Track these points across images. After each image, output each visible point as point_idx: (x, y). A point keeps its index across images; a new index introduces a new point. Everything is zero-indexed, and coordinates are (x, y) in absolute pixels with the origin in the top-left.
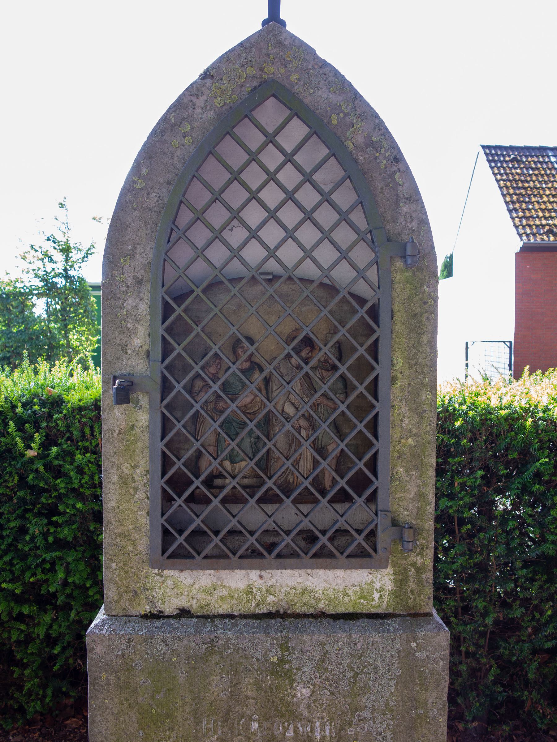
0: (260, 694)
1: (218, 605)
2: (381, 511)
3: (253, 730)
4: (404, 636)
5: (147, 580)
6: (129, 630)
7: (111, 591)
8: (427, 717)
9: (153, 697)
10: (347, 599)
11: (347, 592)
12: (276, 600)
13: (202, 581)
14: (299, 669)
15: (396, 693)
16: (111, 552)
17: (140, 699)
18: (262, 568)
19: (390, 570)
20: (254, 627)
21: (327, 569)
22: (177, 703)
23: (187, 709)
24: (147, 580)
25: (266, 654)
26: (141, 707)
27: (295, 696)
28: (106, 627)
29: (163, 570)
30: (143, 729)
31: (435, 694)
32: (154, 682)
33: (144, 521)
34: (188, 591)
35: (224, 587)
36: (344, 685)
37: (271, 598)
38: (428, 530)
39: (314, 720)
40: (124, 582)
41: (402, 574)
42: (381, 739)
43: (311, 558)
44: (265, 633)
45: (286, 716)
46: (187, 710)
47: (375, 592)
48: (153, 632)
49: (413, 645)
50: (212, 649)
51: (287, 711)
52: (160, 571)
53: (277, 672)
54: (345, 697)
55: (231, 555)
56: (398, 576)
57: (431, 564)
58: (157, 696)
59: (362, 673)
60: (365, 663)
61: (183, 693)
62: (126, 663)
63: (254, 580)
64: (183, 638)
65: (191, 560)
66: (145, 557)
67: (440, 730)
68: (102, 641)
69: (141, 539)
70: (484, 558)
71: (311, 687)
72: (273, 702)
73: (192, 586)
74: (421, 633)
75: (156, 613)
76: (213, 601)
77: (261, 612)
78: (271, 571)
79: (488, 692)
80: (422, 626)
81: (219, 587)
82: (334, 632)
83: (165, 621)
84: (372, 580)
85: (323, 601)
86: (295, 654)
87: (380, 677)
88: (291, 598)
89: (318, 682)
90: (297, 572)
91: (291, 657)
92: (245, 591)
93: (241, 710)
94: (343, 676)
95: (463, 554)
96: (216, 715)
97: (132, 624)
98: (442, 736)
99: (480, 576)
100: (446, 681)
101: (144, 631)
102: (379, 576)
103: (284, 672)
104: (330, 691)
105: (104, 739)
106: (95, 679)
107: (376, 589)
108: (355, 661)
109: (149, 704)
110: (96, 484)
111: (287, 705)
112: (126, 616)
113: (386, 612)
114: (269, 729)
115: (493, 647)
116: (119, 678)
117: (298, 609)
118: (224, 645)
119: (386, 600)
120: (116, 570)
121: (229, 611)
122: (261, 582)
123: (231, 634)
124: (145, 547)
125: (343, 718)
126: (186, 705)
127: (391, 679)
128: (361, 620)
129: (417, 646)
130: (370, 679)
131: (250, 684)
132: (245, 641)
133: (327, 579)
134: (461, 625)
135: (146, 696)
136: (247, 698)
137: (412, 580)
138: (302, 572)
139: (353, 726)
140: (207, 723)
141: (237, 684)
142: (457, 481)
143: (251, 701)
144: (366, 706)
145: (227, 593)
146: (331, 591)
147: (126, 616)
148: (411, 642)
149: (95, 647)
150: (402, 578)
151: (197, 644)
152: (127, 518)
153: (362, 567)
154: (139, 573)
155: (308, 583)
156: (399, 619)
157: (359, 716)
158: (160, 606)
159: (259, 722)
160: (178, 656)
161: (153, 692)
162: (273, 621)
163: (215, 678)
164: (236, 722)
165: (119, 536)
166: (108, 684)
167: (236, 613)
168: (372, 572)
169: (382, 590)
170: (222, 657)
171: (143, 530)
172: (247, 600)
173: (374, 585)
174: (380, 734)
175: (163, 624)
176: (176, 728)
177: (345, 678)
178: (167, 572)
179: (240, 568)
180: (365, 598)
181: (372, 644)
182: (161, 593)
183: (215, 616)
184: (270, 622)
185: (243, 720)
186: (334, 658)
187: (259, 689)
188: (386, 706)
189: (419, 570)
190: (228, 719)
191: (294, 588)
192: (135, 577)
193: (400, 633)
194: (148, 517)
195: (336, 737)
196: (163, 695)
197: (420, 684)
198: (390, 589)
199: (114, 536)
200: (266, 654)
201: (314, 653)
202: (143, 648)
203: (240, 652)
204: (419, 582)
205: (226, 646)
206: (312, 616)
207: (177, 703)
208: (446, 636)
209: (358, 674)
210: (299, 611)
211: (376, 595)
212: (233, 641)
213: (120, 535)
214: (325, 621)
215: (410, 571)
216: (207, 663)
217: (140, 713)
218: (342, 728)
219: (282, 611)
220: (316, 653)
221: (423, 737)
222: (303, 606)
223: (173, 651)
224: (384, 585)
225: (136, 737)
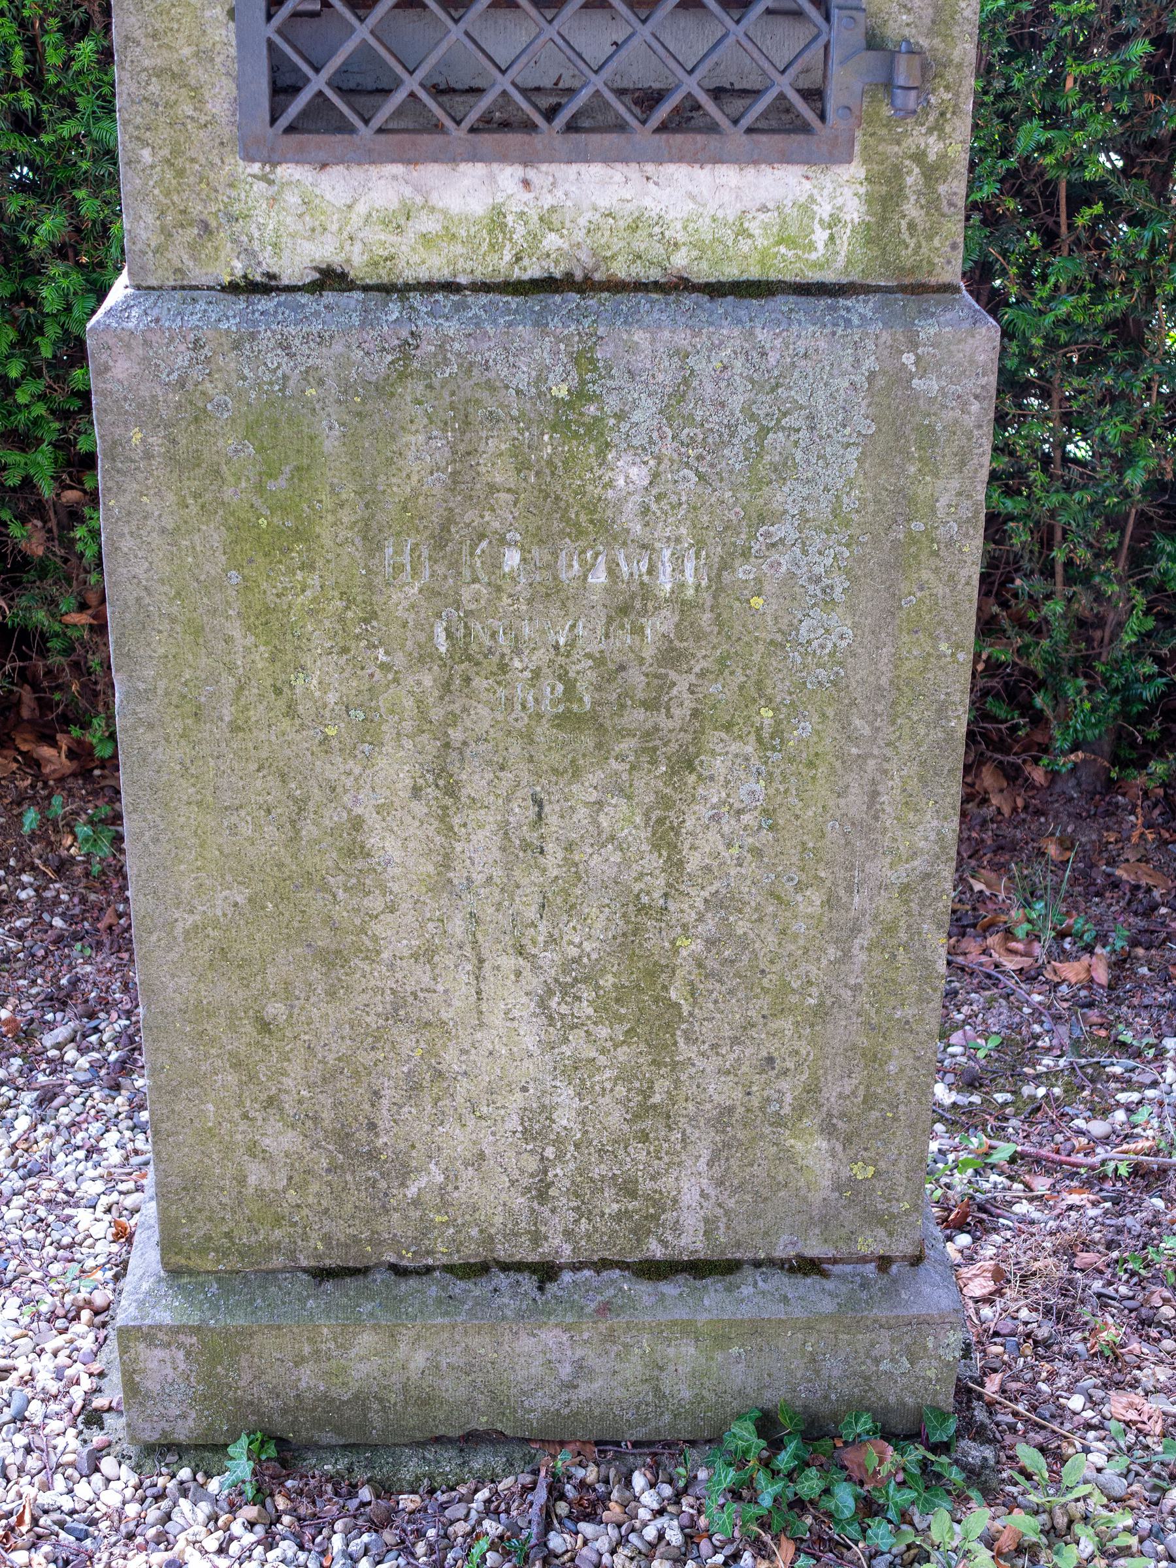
0: (525, 480)
1: (416, 259)
2: (840, 8)
3: (507, 569)
4: (885, 336)
5: (234, 194)
6: (194, 320)
7: (142, 224)
8: (933, 541)
9: (260, 489)
10: (745, 246)
11: (746, 225)
12: (566, 246)
13: (373, 194)
14: (621, 416)
15: (861, 480)
16: (139, 120)
17: (228, 493)
18: (528, 160)
19: (856, 170)
20: (508, 311)
21: (696, 162)
22: (320, 501)
23: (346, 516)
24: (234, 194)
25: (540, 379)
26: (233, 514)
27: (610, 484)
28: (135, 312)
29: (274, 164)
30: (239, 568)
31: (955, 484)
32: (261, 449)
33: (223, 34)
34: (339, 220)
35: (433, 209)
36: (733, 456)
37: (552, 241)
38: (960, 66)
39: (658, 545)
40: (175, 198)
41: (888, 182)
42: (818, 592)
43: (657, 130)
44: (536, 324)
45: (587, 534)
46: (345, 520)
47: (817, 227)
48: (255, 323)
49: (908, 359)
50: (405, 366)
51: (591, 521)
52: (267, 168)
53: (568, 423)
54: (734, 488)
55: (449, 123)
56: (877, 187)
57: (963, 155)
58: (271, 485)
59: (779, 427)
60: (784, 403)
61: (334, 476)
62: (191, 402)
63: (510, 192)
64: (332, 337)
65: (346, 136)
66: (227, 132)
67: (964, 573)
68: (128, 346)
69: (213, 85)
70: (1135, 307)
71: (652, 463)
72: (557, 498)
73: (350, 207)
74: (928, 330)
75: (259, 279)
76: (403, 248)
77: (526, 276)
78: (553, 168)
79: (1117, 681)
80: (933, 315)
81: (418, 211)
82: (712, 324)
83: (282, 298)
84: (811, 197)
85: (684, 250)
86: (612, 377)
87: (821, 438)
88: (603, 241)
89: (668, 449)
90: (618, 172)
91: (603, 386)
92: (485, 221)
93: (477, 520)
94: (732, 436)
95: (1075, 287)
96: (418, 531)
97: (201, 306)
98: (968, 589)
99: (1119, 356)
100: (984, 454)
101: (232, 321)
102: (829, 185)
103: (583, 424)
104: (697, 472)
105: (144, 594)
106: (114, 443)
107: (821, 219)
108: (761, 397)
109: (252, 506)
110: (16, 79)
111: (591, 508)
112: (183, 288)
113: (844, 280)
114: (548, 566)
115: (1139, 559)
116: (174, 442)
117: (621, 270)
118: (435, 355)
119: (843, 247)
120: (152, 167)
121: (445, 274)
122: (527, 196)
123: (451, 328)
124: (226, 106)
125: (727, 541)
126: (342, 506)
127: (848, 445)
128: (780, 299)
129: (916, 363)
130: (796, 442)
131: (501, 454)
132: (486, 346)
133: (695, 191)
134: (1057, 491)
135: (244, 484)
136: (493, 488)
137: (913, 198)
138: (632, 170)
139: (752, 559)
140: (395, 552)
141: (469, 453)
142: (1075, 70)
143: (503, 496)
144: (785, 512)
145: (438, 227)
146: (704, 224)
147: (183, 288)
148: (902, 352)
149: (111, 363)
150: (888, 192)
151: (368, 354)
152: (176, 26)
153: (786, 159)
154: (212, 175)
155: (648, 202)
156: (874, 299)
157: (768, 535)
158: (269, 262)
159: (522, 549)
160: (321, 382)
161: (260, 474)
162: (558, 298)
163: (413, 439)
164: (466, 549)
165: (158, 76)
166: (148, 456)
167: (463, 280)
168: (810, 174)
169: (834, 222)
170: (430, 387)
171: (218, 60)
172: (492, 246)
173: (815, 208)
174: (818, 580)
175: (279, 304)
176: (319, 564)
177: (735, 441)
178: (285, 171)
179: (474, 157)
180: (791, 242)
181: (806, 355)
182: (271, 227)
183: (408, 288)
184: (550, 301)
185: (484, 544)
186: (709, 388)
187: (522, 466)
188: (833, 511)
189: (933, 173)
190: (447, 541)
191: (610, 215)
192: (203, 186)
193: (875, 328)
194: (232, 25)
195: (709, 587)
196: (284, 483)
197: (921, 459)
198: (856, 220)
199: (144, 76)
200: (540, 379)
201: (660, 377)
202: (233, 365)
203: (475, 372)
204: (932, 204)
205: (440, 358)
206: (657, 286)
207: (320, 501)
208: (991, 339)
209: (769, 430)
210: (622, 275)
211: (820, 236)
212: (457, 346)
213: (159, 73)
214: (689, 300)
215: (909, 173)
216: (394, 402)
217: (229, 529)
218: (725, 566)
219: (579, 275)
220: (666, 378)
221: (921, 589)
222: (634, 262)
223: (307, 372)
224: (840, 209)
225: (221, 586)
